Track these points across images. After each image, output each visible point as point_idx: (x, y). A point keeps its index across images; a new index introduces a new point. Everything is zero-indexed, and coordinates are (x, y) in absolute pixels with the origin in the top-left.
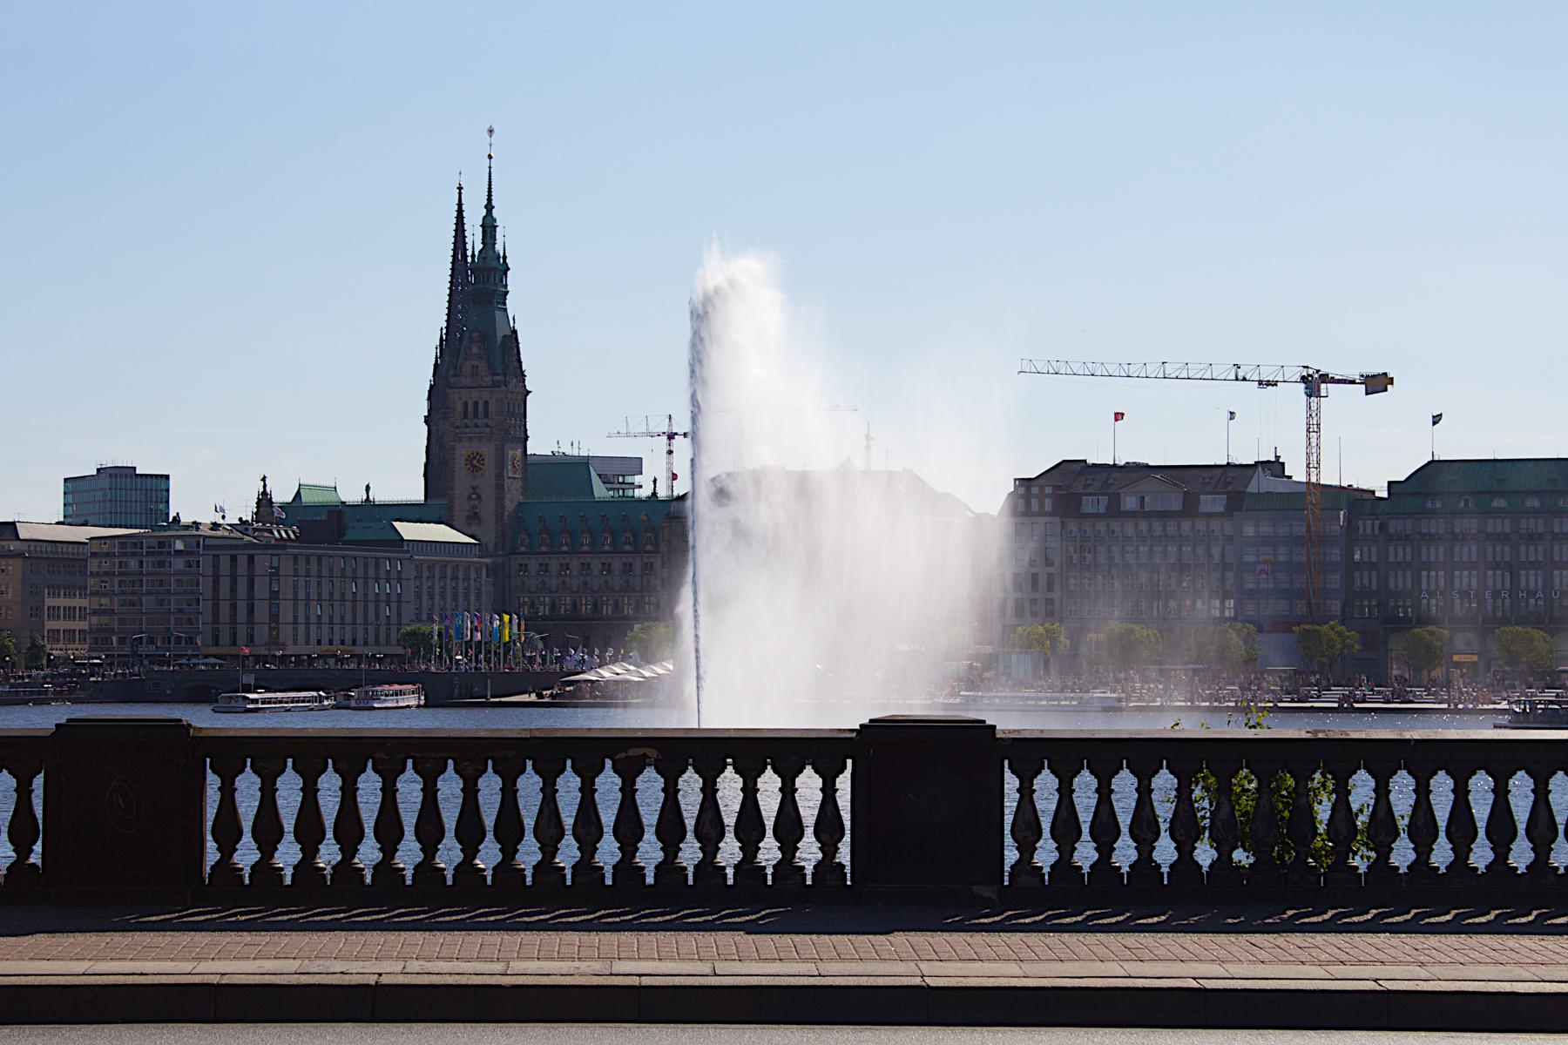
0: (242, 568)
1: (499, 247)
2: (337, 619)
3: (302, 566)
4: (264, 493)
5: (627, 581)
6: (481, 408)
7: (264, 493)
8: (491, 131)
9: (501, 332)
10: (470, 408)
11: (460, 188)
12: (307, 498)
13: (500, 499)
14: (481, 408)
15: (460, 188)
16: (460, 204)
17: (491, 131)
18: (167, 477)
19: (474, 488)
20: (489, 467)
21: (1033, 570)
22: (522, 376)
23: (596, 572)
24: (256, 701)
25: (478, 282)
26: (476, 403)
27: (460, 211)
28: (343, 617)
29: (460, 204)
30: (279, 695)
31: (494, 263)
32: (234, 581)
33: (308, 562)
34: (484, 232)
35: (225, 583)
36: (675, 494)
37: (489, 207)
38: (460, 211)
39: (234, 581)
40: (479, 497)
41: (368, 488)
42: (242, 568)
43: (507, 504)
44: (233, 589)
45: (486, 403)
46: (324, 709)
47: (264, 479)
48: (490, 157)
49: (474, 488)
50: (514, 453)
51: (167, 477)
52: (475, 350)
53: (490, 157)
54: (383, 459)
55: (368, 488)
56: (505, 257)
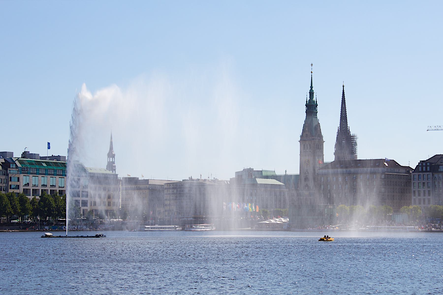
1: (314, 99)
8: (312, 65)
9: (315, 124)
11: (343, 86)
15: (343, 86)
16: (343, 91)
17: (312, 65)
21: (71, 170)
24: (148, 228)
29: (343, 91)
30: (159, 226)
31: (313, 104)
34: (310, 94)
37: (311, 87)
40: (308, 173)
46: (177, 231)
48: (312, 72)
52: (307, 129)
53: (312, 72)
56: (316, 102)
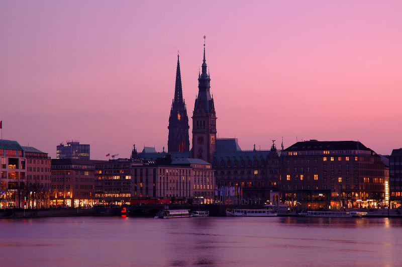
1: (207, 73)
4: (134, 150)
5: (229, 177)
6: (202, 123)
7: (134, 150)
8: (205, 37)
10: (199, 123)
11: (178, 56)
12: (147, 151)
13: (208, 152)
14: (202, 123)
16: (178, 61)
17: (205, 37)
19: (200, 148)
22: (214, 113)
23: (232, 174)
26: (201, 122)
27: (178, 63)
29: (178, 61)
36: (284, 149)
38: (178, 63)
40: (202, 151)
41: (255, 145)
43: (211, 152)
47: (134, 145)
48: (204, 45)
49: (200, 148)
50: (212, 137)
53: (204, 45)
55: (255, 145)
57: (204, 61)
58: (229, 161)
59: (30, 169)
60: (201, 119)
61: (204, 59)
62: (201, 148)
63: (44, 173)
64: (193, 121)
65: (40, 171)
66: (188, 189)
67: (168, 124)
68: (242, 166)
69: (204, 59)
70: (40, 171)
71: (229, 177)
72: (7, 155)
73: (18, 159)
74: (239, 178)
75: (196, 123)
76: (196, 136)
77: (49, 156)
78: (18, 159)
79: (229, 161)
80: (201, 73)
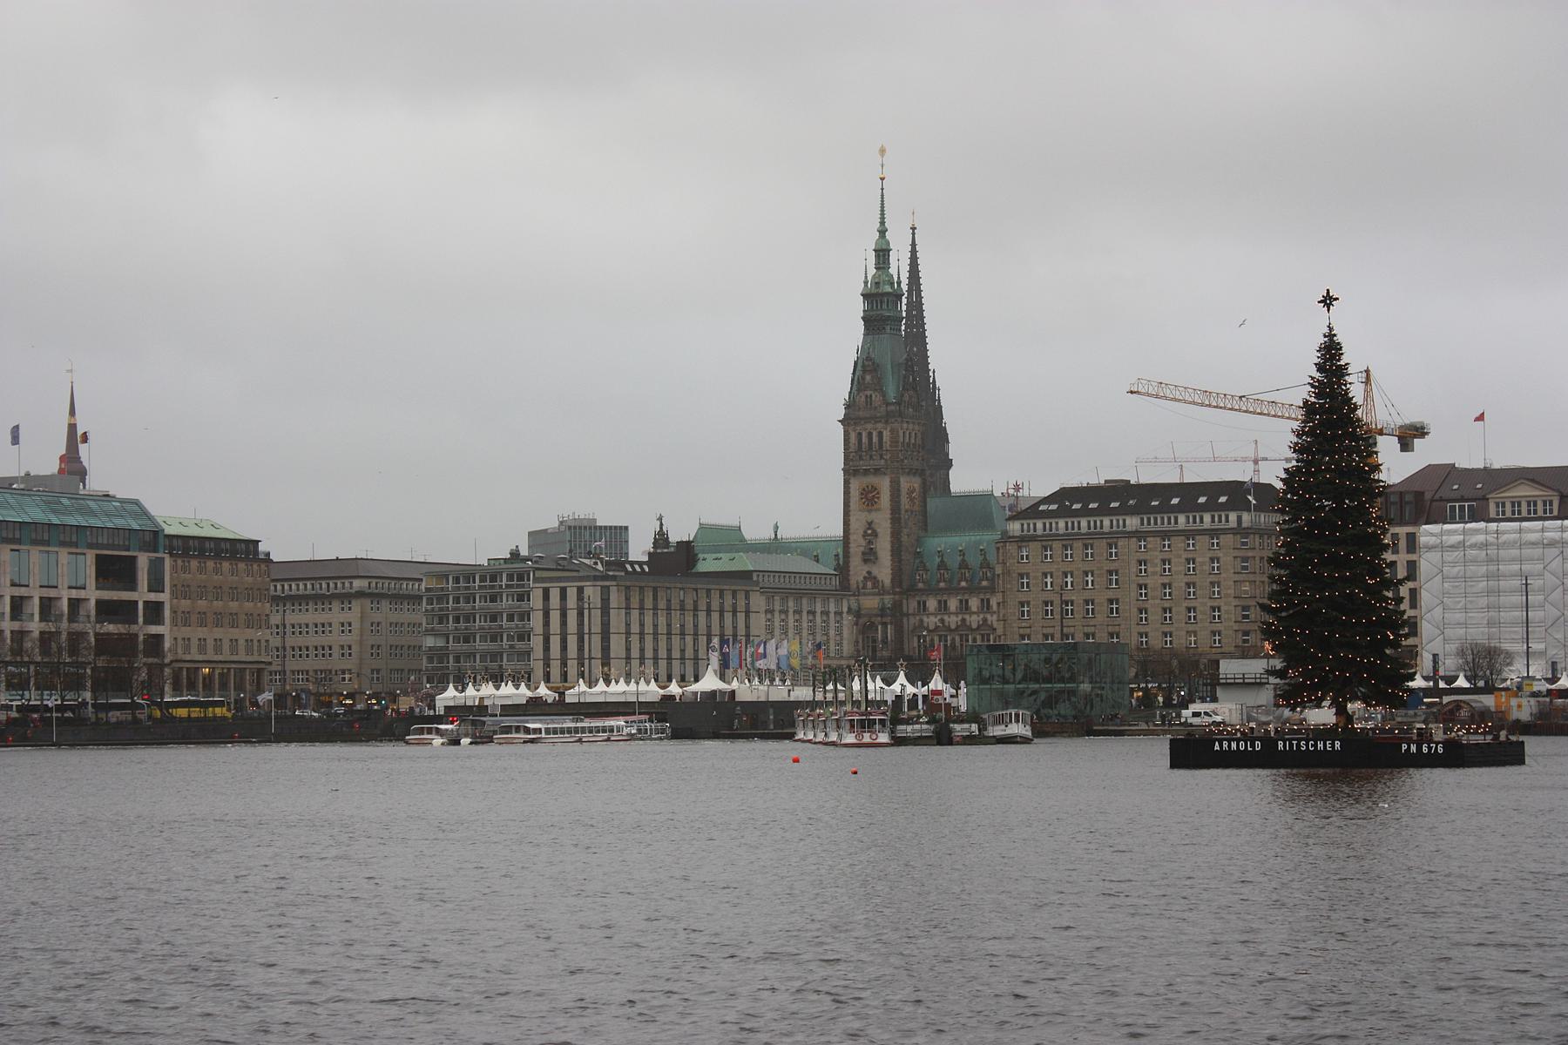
0: (572, 601)
2: (676, 654)
3: (728, 601)
6: (875, 439)
8: (882, 151)
11: (913, 229)
15: (913, 229)
16: (914, 245)
17: (882, 151)
18: (626, 528)
20: (885, 499)
25: (892, 315)
26: (870, 434)
28: (683, 651)
29: (914, 245)
32: (564, 615)
33: (734, 597)
34: (877, 257)
35: (555, 617)
39: (564, 615)
40: (875, 534)
41: (776, 527)
42: (572, 601)
43: (904, 538)
44: (564, 623)
45: (880, 434)
49: (870, 524)
51: (626, 528)
54: (797, 496)
57: (883, 232)
58: (964, 565)
59: (180, 591)
60: (869, 426)
61: (882, 223)
62: (870, 524)
63: (1178, 566)
64: (846, 434)
65: (242, 642)
66: (635, 639)
67: (841, 413)
68: (942, 585)
69: (882, 223)
70: (242, 642)
71: (963, 620)
72: (91, 546)
73: (135, 558)
74: (974, 626)
75: (853, 436)
76: (855, 485)
77: (262, 548)
78: (135, 558)
79: (964, 565)
80: (872, 271)
